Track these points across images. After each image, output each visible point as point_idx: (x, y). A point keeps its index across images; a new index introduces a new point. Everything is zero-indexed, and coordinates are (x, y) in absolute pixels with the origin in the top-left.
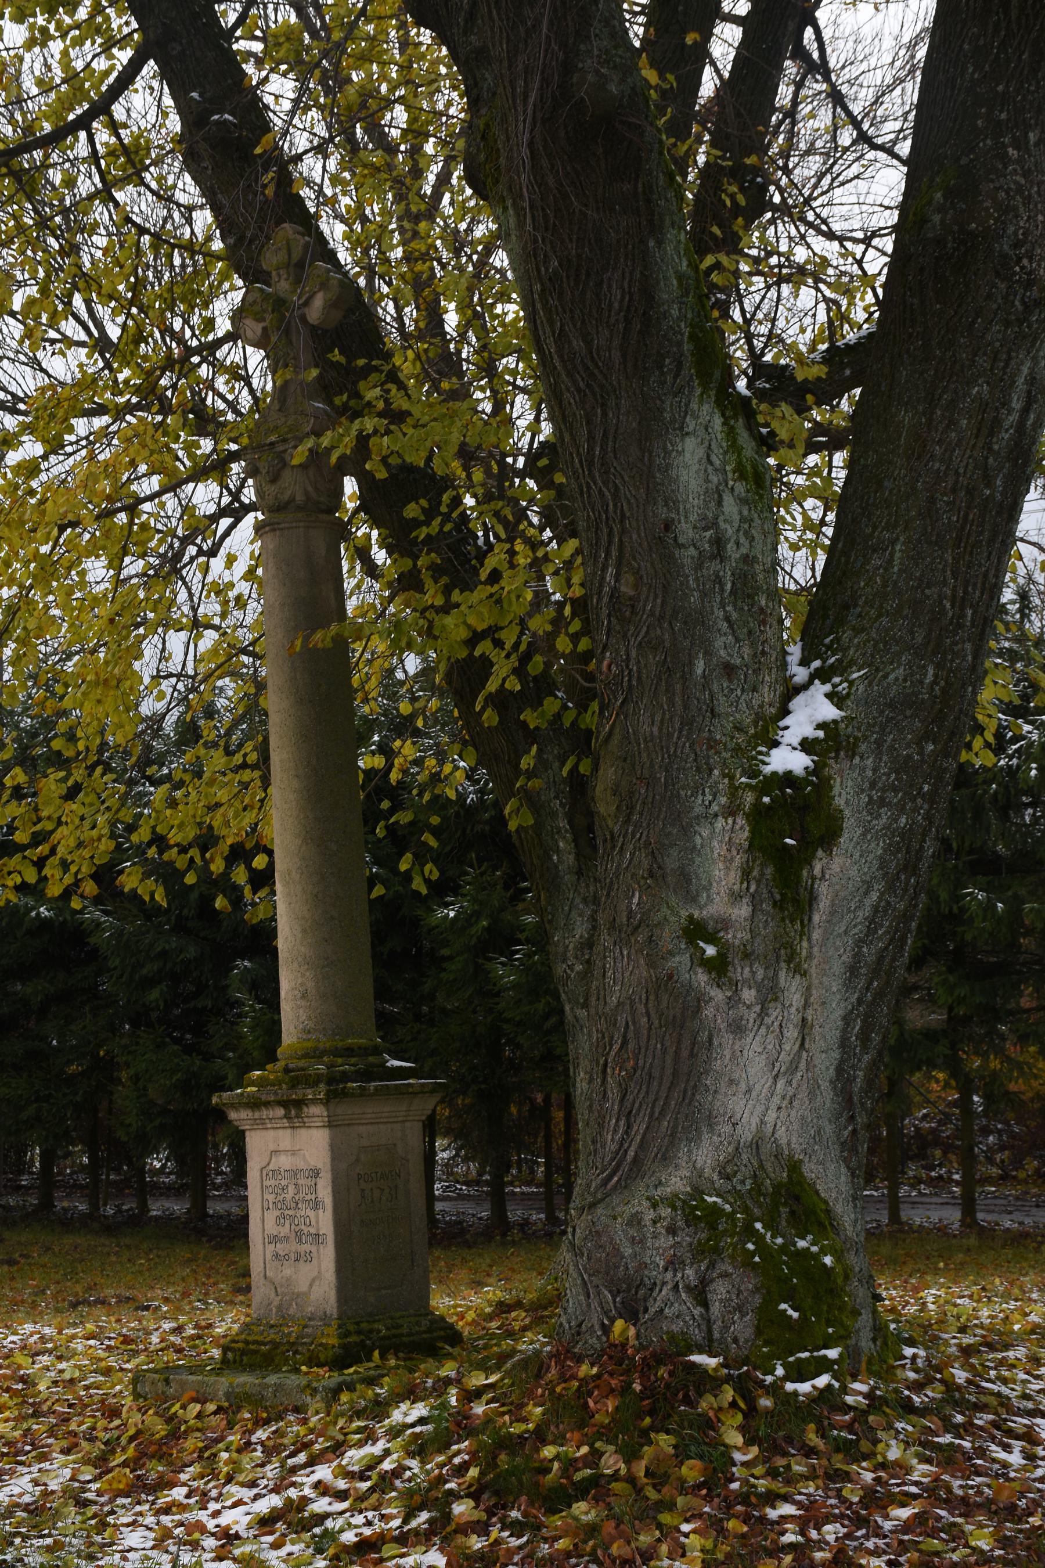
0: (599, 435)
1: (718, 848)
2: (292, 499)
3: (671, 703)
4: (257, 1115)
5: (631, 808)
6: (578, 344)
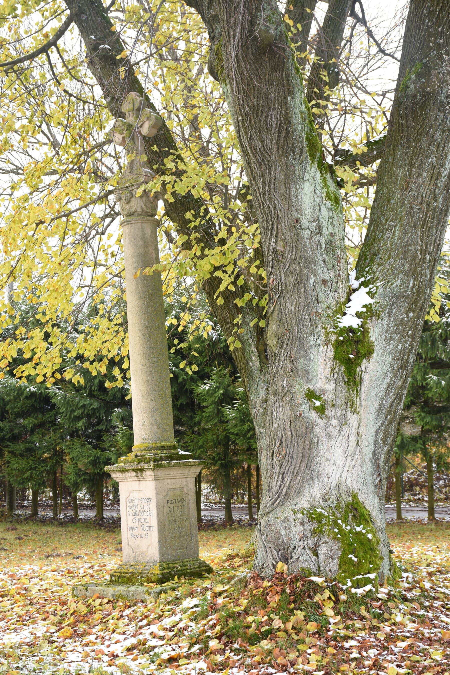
0: (267, 182)
3: (300, 297)
4: (124, 475)
5: (283, 342)
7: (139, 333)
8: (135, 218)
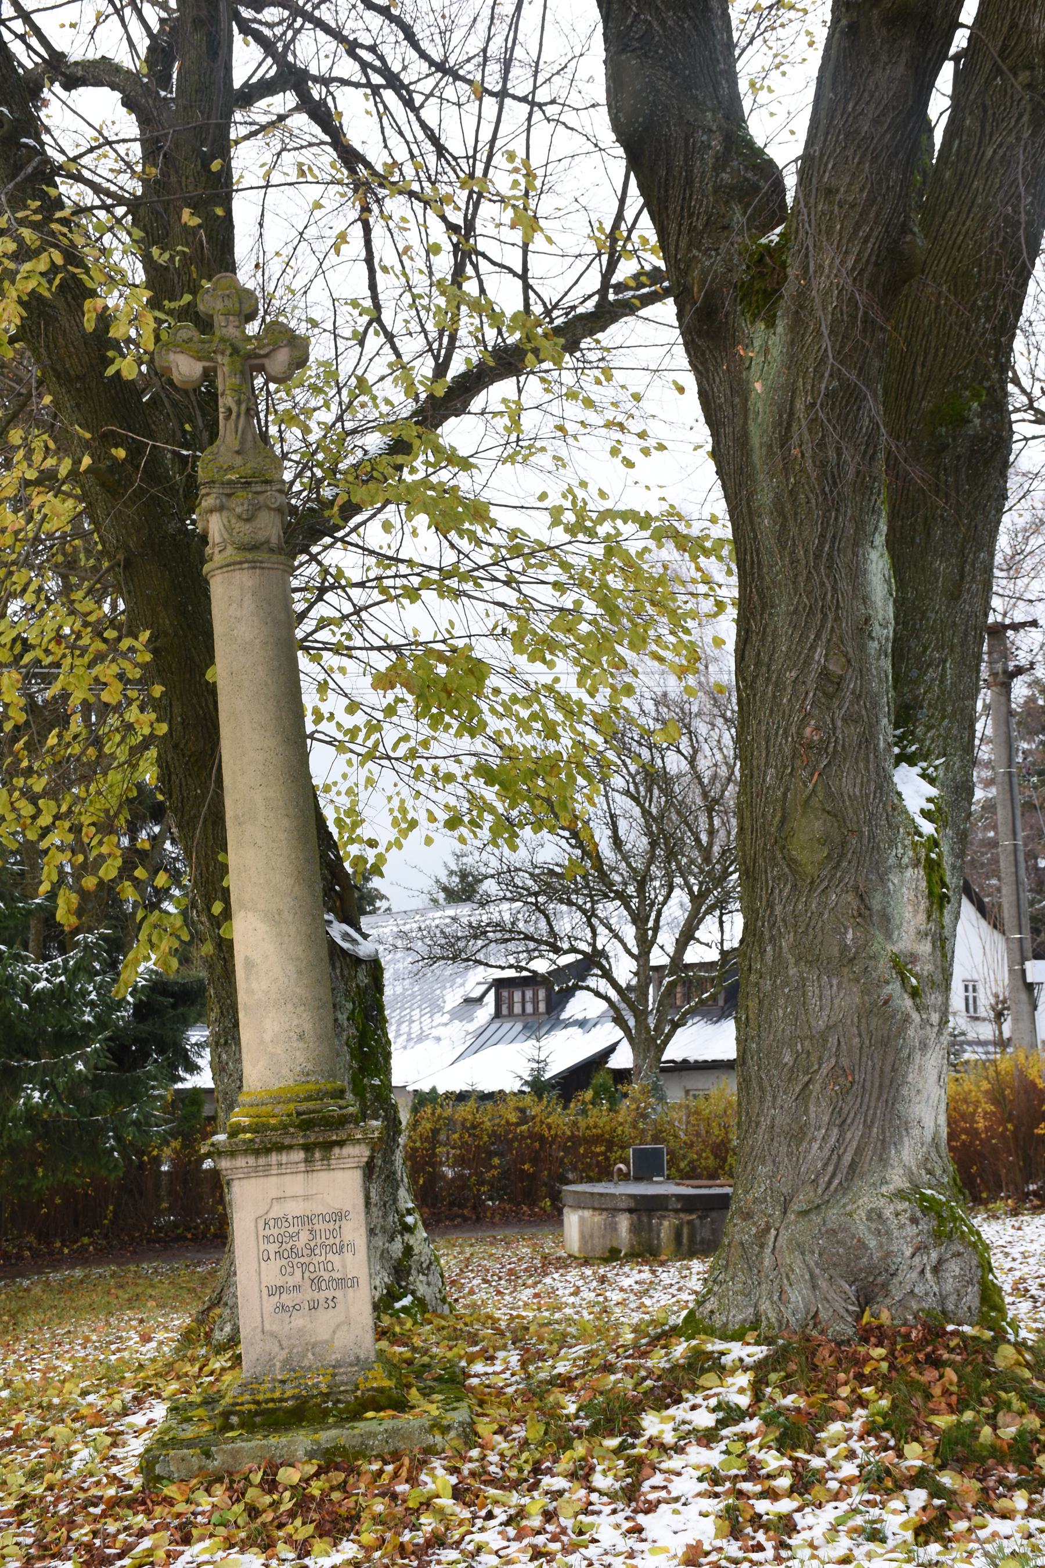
0: (829, 536)
1: (907, 894)
2: (268, 542)
3: (867, 769)
4: (262, 1161)
5: (842, 856)
6: (832, 454)
7: (286, 823)
8: (262, 555)
